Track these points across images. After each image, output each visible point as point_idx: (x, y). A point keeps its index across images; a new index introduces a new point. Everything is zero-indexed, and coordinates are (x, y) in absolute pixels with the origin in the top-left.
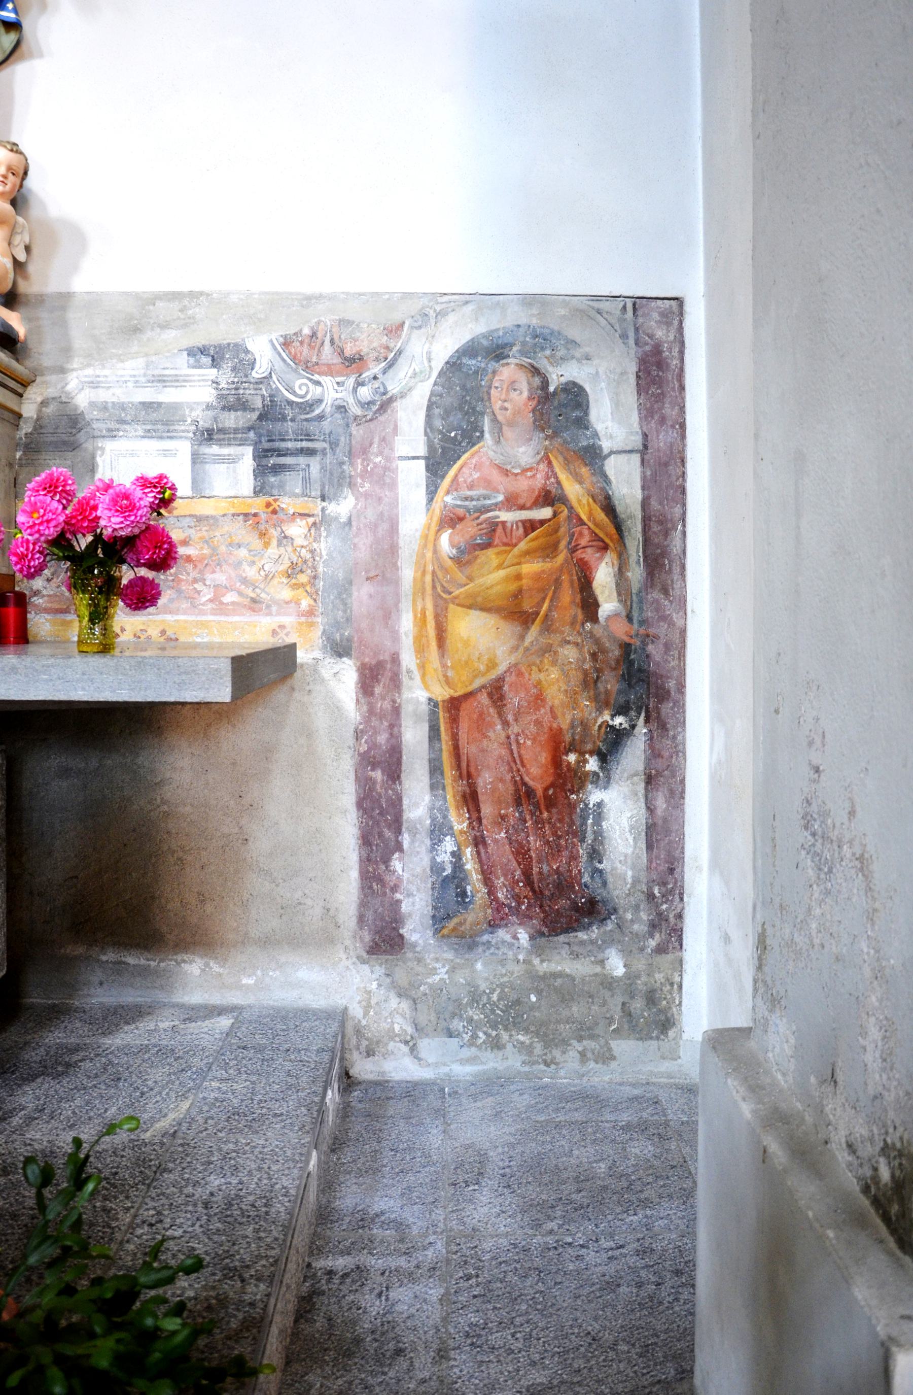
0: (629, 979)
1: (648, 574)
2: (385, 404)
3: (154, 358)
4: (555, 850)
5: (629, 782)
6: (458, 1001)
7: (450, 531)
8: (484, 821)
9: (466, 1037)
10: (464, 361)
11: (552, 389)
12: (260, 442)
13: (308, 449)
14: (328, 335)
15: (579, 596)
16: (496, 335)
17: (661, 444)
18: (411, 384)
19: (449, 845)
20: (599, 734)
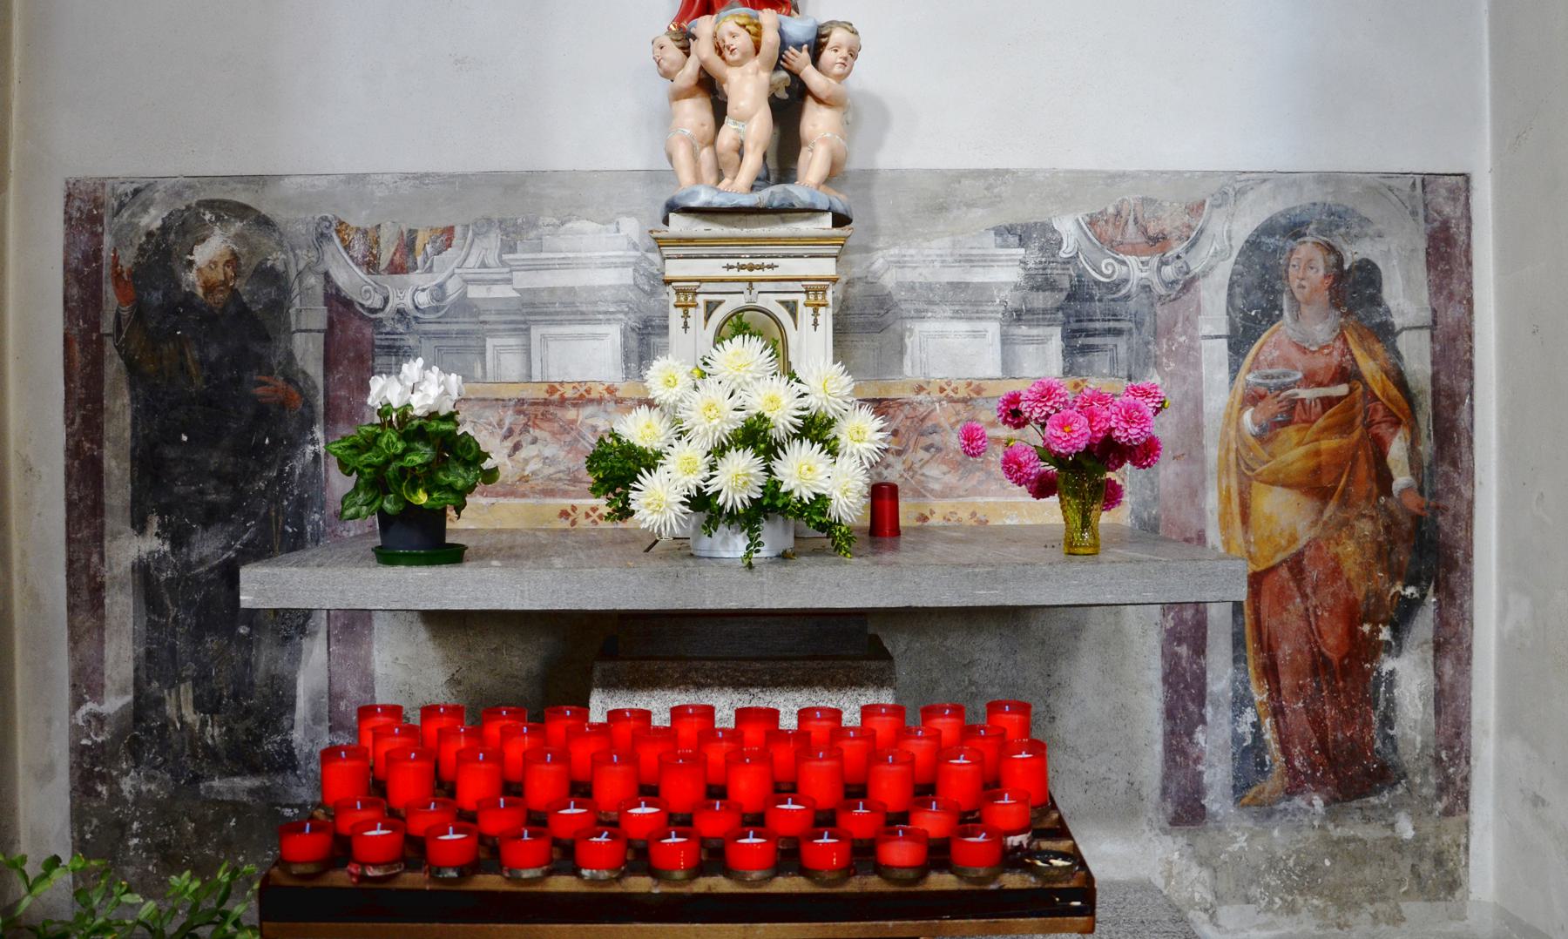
0: (1418, 841)
1: (1438, 448)
2: (1188, 284)
3: (960, 238)
4: (1348, 718)
5: (1419, 650)
6: (1256, 867)
7: (1252, 409)
8: (1284, 692)
9: (1263, 903)
10: (1263, 239)
11: (1346, 267)
12: (1069, 322)
13: (1115, 329)
14: (1132, 213)
15: (1374, 471)
16: (1293, 213)
17: (1450, 320)
18: (1212, 263)
19: (1249, 716)
20: (1392, 604)
